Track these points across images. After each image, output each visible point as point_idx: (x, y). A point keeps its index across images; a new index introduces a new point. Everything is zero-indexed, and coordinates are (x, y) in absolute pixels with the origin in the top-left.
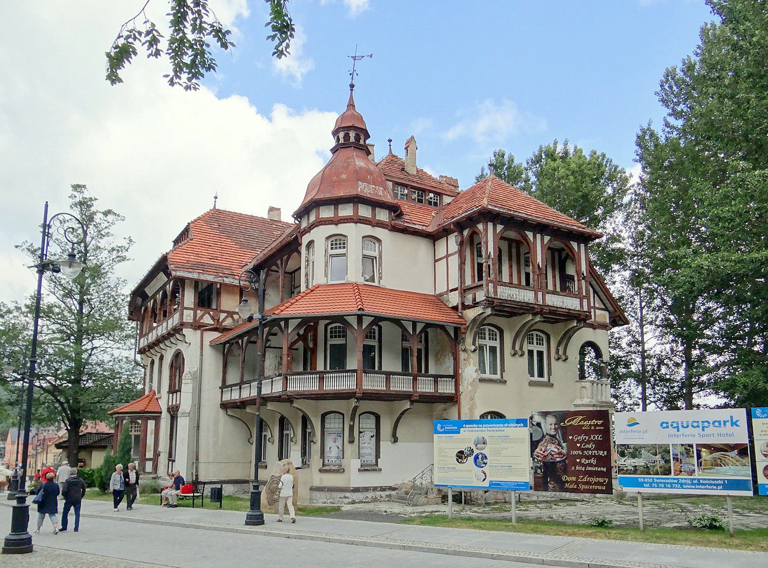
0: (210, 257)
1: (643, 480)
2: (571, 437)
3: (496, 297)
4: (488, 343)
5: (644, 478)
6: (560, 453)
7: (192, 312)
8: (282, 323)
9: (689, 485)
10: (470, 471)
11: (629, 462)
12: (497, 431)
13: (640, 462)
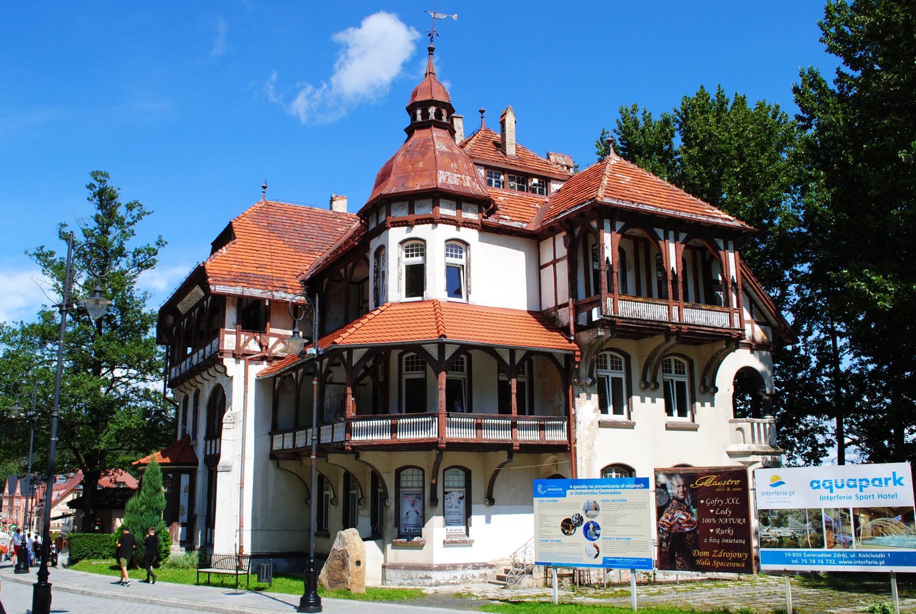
0: (257, 266)
1: (790, 555)
2: (702, 502)
3: (616, 315)
4: (610, 373)
5: (791, 552)
6: (689, 522)
7: (234, 337)
8: (345, 353)
9: (846, 560)
10: (579, 545)
11: (774, 532)
12: (611, 493)
13: (786, 532)
